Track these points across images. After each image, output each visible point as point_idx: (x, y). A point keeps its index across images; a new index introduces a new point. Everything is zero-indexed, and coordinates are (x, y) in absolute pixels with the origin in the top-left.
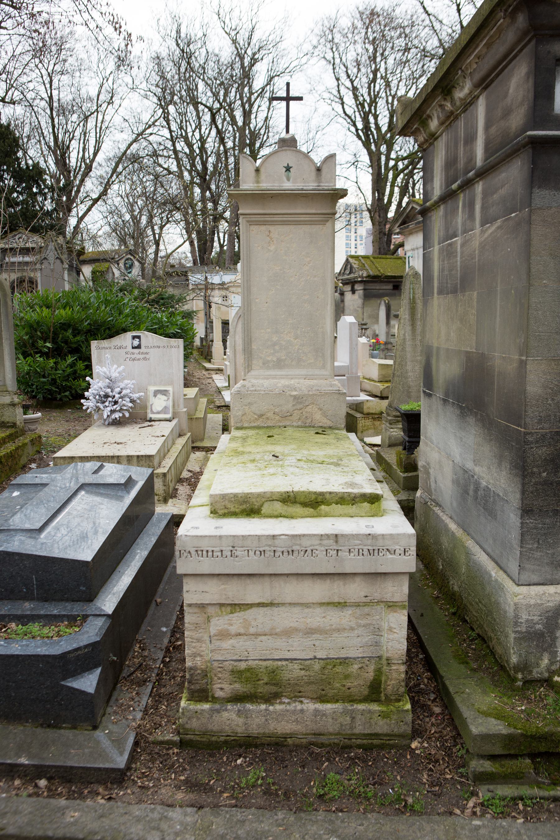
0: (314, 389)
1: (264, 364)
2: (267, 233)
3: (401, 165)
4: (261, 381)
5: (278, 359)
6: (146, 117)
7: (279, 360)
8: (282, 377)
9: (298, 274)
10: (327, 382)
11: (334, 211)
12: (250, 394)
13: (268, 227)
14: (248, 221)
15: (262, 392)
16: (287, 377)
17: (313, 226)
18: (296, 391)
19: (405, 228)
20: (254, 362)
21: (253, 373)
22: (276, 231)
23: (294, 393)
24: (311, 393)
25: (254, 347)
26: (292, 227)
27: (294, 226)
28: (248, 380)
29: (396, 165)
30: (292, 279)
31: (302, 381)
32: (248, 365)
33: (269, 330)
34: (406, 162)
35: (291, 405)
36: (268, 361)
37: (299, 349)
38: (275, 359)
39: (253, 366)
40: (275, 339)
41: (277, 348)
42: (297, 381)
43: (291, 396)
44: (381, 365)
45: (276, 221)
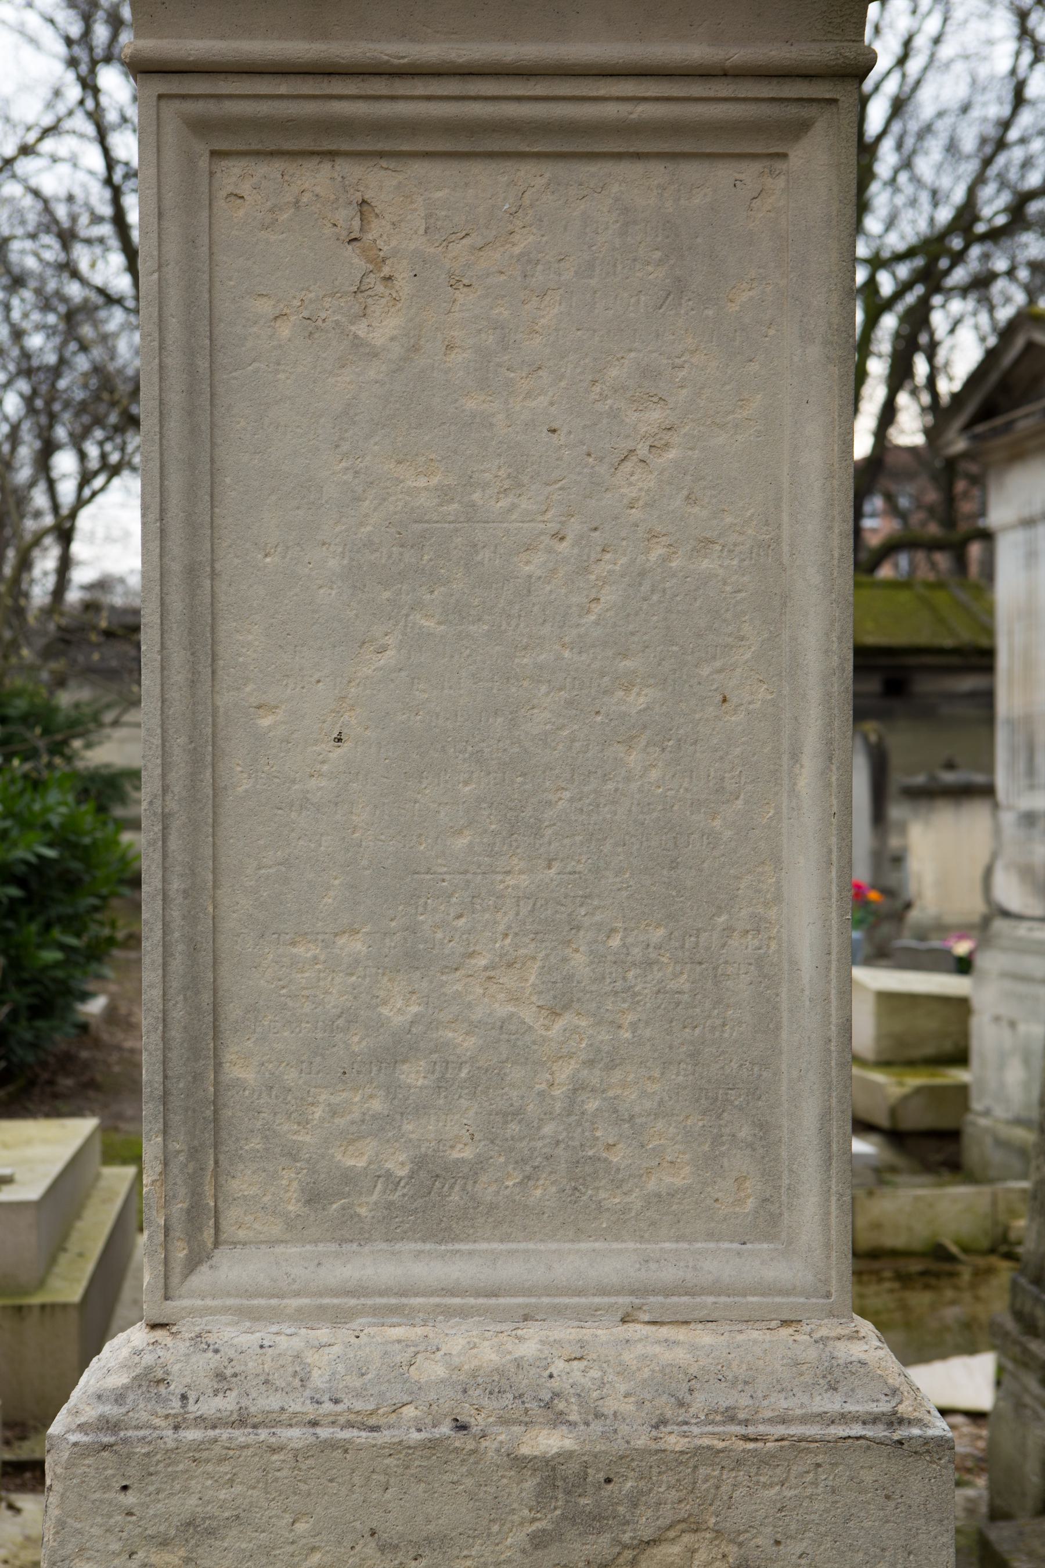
0: (699, 1402)
1: (314, 1198)
2: (346, 216)
3: (886, 285)
4: (289, 1339)
5: (420, 1163)
6: (32, 111)
7: (432, 1174)
8: (452, 1303)
9: (575, 527)
10: (796, 1343)
11: (849, 52)
12: (197, 1452)
13: (344, 168)
14: (200, 127)
15: (295, 1436)
16: (482, 1302)
17: (691, 171)
18: (559, 1420)
19: (996, 432)
20: (243, 1183)
21: (229, 1269)
22: (414, 201)
23: (549, 1442)
24: (674, 1441)
25: (242, 1068)
26: (533, 176)
27: (549, 170)
28: (187, 1329)
29: (871, 284)
30: (533, 565)
31: (604, 1334)
32: (194, 1215)
33: (357, 946)
34: (903, 271)
35: (518, 1537)
36: (349, 1178)
37: (578, 1088)
38: (398, 1164)
39: (231, 1215)
40: (399, 1009)
41: (414, 1075)
42: (565, 1332)
43: (520, 1463)
44: (887, 1000)
45: (413, 127)
